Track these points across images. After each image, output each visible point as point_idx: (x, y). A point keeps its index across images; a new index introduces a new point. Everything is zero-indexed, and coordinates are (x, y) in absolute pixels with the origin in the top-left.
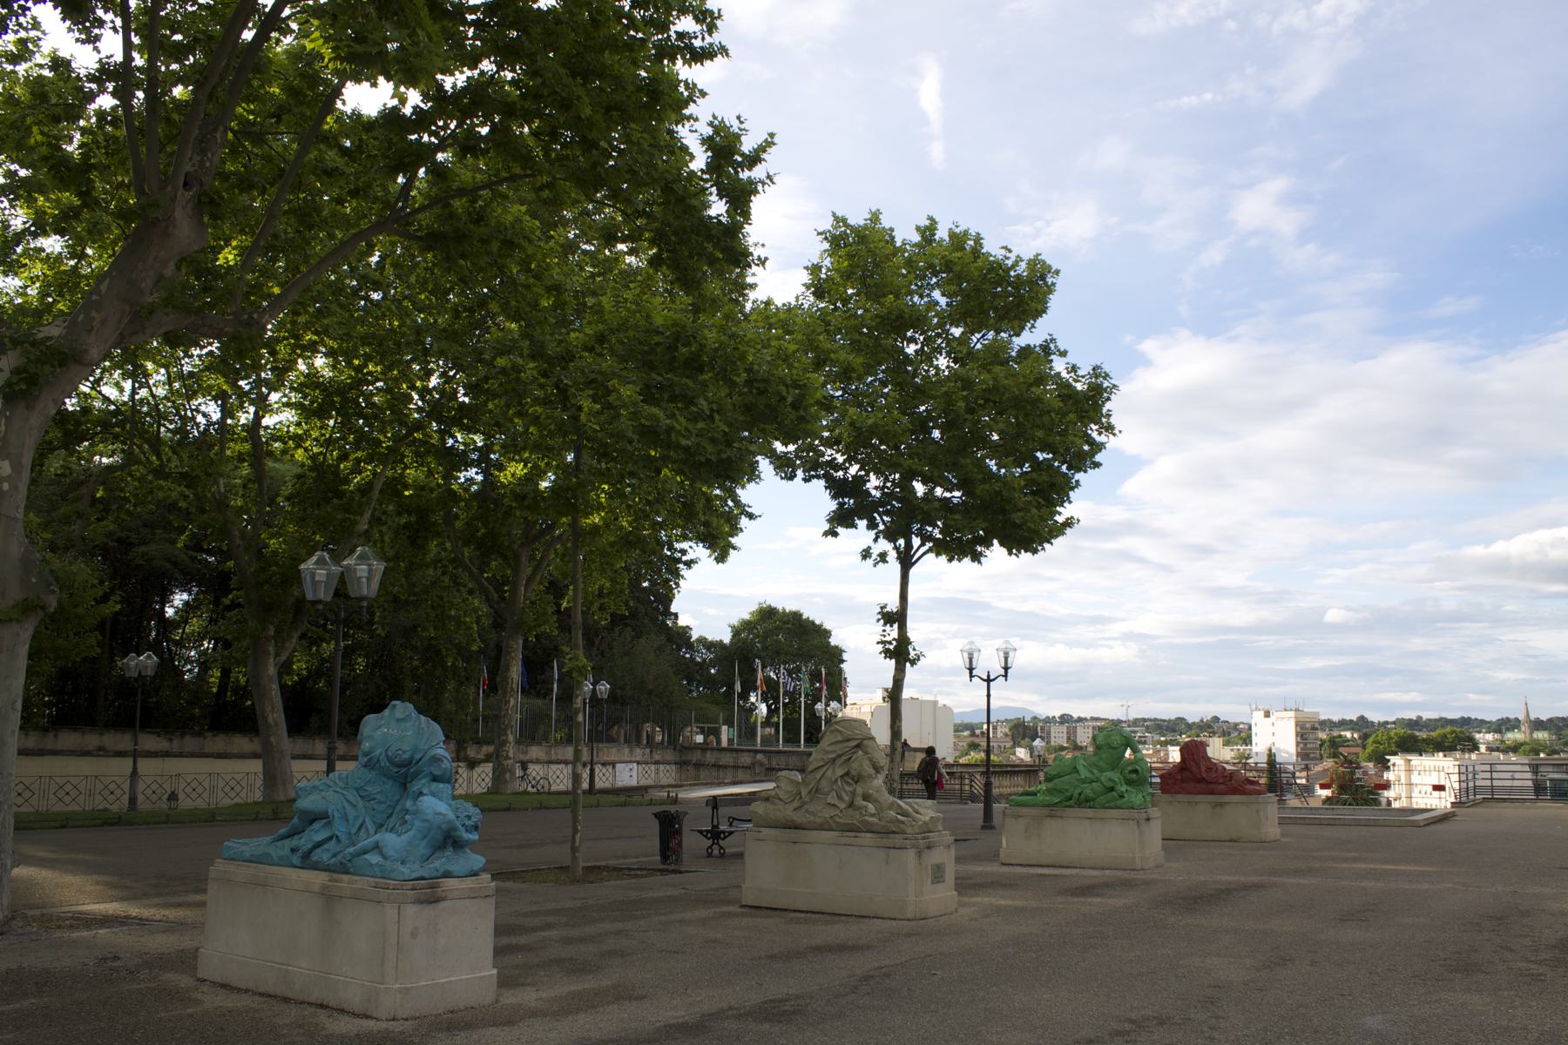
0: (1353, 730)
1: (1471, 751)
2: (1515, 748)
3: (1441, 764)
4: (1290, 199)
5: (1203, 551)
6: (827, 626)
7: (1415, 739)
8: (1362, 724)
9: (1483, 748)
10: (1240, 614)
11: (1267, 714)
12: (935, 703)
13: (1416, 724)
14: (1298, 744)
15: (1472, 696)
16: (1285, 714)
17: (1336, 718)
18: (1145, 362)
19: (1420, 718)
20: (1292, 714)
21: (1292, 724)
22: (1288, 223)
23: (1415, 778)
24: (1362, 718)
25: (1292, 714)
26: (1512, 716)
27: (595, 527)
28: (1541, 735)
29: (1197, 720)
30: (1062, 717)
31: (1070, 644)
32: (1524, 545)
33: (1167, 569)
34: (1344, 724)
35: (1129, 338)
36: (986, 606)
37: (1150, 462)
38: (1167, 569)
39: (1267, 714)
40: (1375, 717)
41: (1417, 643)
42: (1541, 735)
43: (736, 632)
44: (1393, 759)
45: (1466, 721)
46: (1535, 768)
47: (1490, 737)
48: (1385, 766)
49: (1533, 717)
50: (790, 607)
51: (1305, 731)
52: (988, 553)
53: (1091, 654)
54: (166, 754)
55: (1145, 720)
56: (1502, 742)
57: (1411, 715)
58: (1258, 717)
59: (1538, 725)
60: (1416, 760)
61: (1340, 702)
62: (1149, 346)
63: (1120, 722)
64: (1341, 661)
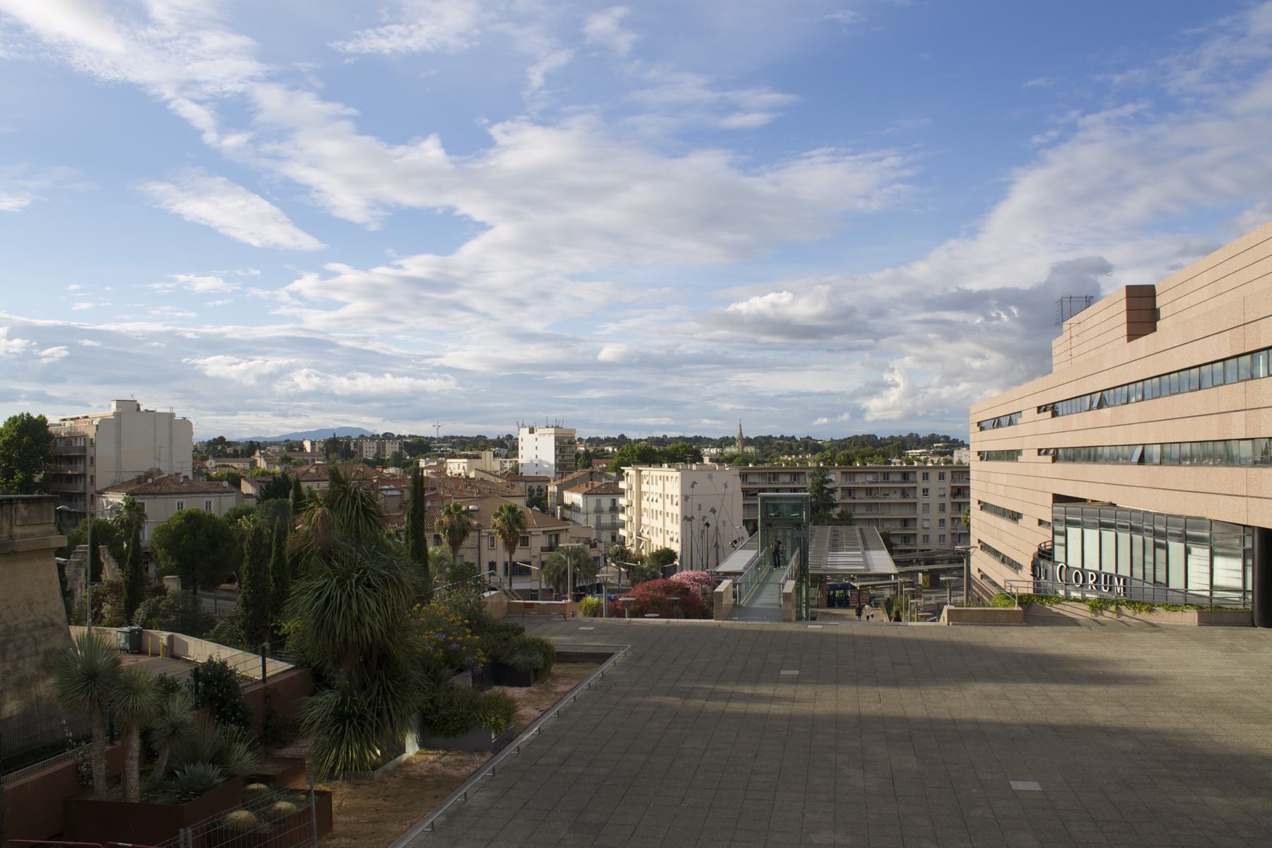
0: (614, 445)
1: (693, 462)
2: (730, 460)
3: (666, 474)
4: (625, 24)
5: (519, 304)
9: (706, 460)
10: (533, 353)
11: (532, 431)
13: (662, 441)
14: (556, 456)
15: (706, 421)
16: (546, 430)
17: (602, 437)
20: (552, 430)
21: (552, 438)
22: (624, 42)
24: (622, 436)
25: (552, 430)
26: (730, 436)
27: (608, 453)
28: (750, 449)
30: (385, 434)
31: (395, 375)
32: (758, 304)
33: (486, 315)
34: (609, 441)
35: (486, 121)
36: (333, 345)
37: (490, 228)
38: (486, 315)
39: (532, 431)
40: (632, 435)
41: (674, 381)
42: (750, 449)
44: (628, 470)
45: (698, 440)
46: (744, 477)
47: (714, 451)
49: (745, 436)
50: (308, 423)
51: (564, 444)
53: (421, 383)
55: (452, 437)
56: (722, 454)
58: (524, 432)
59: (748, 442)
60: (646, 471)
62: (496, 131)
63: (432, 439)
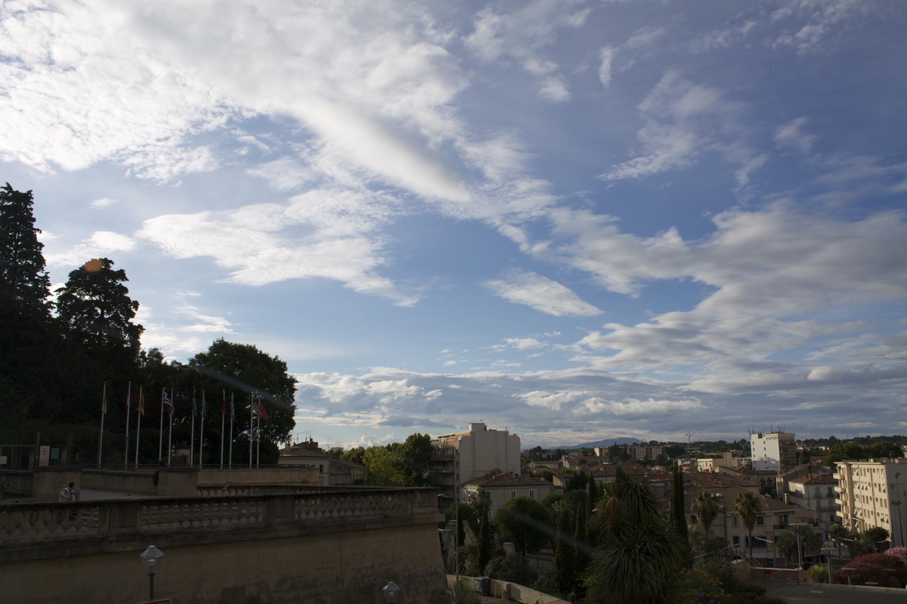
0: (826, 445)
1: (895, 457)
3: (873, 467)
5: (744, 342)
6: (282, 359)
7: (860, 450)
8: (832, 441)
11: (760, 436)
12: (506, 433)
13: (867, 440)
16: (772, 436)
17: (816, 439)
18: (439, 109)
19: (868, 437)
20: (776, 435)
21: (777, 441)
23: (855, 478)
24: (832, 438)
25: (776, 435)
29: (732, 442)
34: (822, 442)
40: (841, 437)
41: (872, 393)
43: (192, 362)
45: (897, 438)
48: (834, 469)
51: (786, 445)
52: (32, 206)
54: (271, 487)
55: (700, 443)
57: (863, 435)
61: (812, 427)
63: (686, 444)
64: (825, 404)
